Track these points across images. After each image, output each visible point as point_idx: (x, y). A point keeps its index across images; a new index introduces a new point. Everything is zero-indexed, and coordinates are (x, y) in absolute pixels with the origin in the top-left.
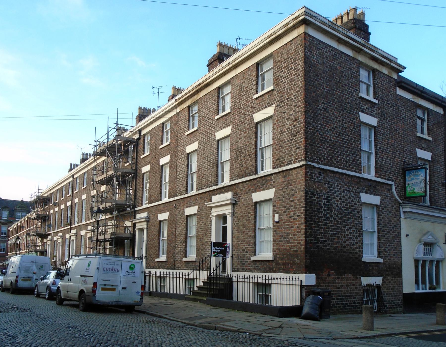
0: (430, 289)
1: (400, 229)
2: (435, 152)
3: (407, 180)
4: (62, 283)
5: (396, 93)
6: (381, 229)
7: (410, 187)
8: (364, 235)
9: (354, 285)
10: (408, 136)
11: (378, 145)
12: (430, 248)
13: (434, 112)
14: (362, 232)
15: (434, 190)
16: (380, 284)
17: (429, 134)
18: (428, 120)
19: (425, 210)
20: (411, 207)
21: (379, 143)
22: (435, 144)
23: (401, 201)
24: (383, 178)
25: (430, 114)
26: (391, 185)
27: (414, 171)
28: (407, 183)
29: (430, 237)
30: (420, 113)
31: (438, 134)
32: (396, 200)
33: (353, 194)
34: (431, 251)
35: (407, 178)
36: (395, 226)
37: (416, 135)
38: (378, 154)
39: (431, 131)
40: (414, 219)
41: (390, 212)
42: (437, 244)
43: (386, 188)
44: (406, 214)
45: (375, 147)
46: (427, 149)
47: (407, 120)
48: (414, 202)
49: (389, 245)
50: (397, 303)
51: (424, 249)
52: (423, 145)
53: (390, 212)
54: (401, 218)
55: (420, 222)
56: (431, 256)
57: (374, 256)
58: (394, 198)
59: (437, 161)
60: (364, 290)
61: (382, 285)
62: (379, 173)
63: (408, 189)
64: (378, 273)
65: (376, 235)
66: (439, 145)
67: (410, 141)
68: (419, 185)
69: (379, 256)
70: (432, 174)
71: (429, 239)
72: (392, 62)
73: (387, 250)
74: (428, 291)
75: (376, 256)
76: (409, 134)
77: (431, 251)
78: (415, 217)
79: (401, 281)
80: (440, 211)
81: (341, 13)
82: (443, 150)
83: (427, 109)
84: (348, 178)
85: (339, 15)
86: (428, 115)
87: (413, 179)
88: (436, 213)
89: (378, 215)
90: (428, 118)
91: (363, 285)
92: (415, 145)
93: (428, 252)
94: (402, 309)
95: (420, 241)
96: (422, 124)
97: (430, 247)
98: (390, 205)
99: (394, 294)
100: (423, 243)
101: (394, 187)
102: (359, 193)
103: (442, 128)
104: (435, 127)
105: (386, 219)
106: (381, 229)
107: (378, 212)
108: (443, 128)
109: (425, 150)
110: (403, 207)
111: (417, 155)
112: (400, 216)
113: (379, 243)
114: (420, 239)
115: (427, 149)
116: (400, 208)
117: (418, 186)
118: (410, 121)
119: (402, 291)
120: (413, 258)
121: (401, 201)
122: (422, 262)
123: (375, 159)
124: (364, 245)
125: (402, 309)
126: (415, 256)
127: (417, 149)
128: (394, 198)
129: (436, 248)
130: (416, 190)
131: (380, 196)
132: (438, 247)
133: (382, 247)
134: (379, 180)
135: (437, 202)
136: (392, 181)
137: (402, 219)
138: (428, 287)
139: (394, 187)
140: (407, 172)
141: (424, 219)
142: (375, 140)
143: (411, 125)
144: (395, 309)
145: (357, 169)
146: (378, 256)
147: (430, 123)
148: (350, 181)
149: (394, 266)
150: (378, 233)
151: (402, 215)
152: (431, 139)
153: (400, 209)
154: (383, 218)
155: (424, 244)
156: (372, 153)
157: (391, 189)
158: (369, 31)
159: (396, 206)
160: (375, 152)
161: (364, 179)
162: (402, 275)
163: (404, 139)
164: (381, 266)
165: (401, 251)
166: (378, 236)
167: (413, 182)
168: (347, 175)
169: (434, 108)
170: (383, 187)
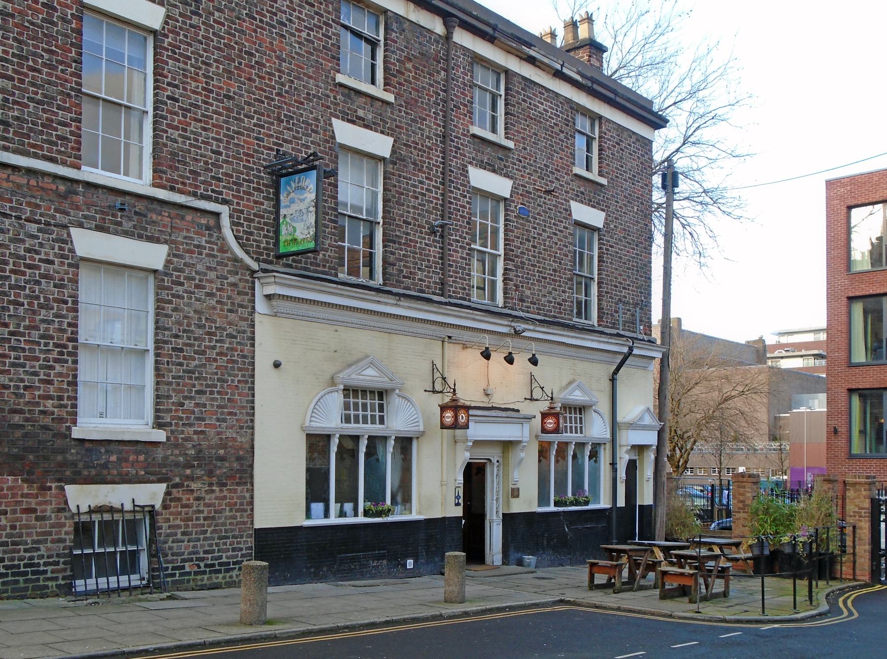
0: (366, 513)
1: (253, 345)
2: (408, 136)
3: (282, 204)
4: (195, 485)
6: (166, 342)
7: (287, 223)
8: (83, 357)
9: (29, 511)
10: (299, 79)
11: (166, 90)
12: (578, 416)
13: (406, 25)
14: (75, 348)
15: (400, 243)
16: (153, 506)
18: (386, 45)
19: (342, 295)
20: (277, 280)
21: (169, 84)
22: (407, 113)
23: (255, 266)
24: (181, 192)
25: (394, 26)
26: (217, 215)
27: (296, 177)
28: (283, 211)
29: (577, 393)
30: (582, 123)
31: (424, 88)
32: (236, 259)
33: (33, 228)
34: (581, 423)
35: (282, 198)
36: (230, 336)
37: (572, 171)
39: (395, 76)
41: (210, 295)
42: (594, 407)
43: (193, 222)
44: (274, 303)
45: (156, 95)
46: (374, 123)
47: (300, 31)
48: (317, 272)
49: (199, 392)
50: (227, 557)
52: (361, 113)
53: (210, 295)
54: (256, 315)
56: (581, 432)
57: (144, 422)
58: (229, 255)
59: (414, 164)
60: (76, 523)
61: (165, 506)
62: (165, 173)
63: (283, 230)
64: (146, 473)
65: (150, 359)
66: (425, 120)
67: (308, 94)
68: (305, 217)
69: (159, 424)
70: (394, 197)
71: (369, 377)
73: (189, 405)
74: (552, 508)
75: (150, 424)
76: (304, 74)
77: (581, 423)
78: (311, 314)
80: (399, 300)
82: (437, 135)
83: (507, 71)
84: (12, 177)
86: (386, 29)
87: (292, 201)
88: (386, 304)
89: (160, 302)
90: (386, 39)
91: (74, 510)
92: (329, 107)
93: (574, 425)
95: (332, 382)
96: (589, 149)
97: (580, 414)
98: (212, 275)
99: (214, 531)
100: (342, 387)
101: (225, 221)
102: (65, 227)
103: (438, 72)
104: (409, 66)
105: (192, 314)
106: (166, 342)
107: (160, 287)
108: (443, 73)
109: (366, 126)
110: (262, 281)
111: (333, 137)
112: (253, 308)
113: (158, 383)
114: (332, 378)
115: (374, 123)
116: (253, 283)
117: (302, 220)
118: (309, 35)
119: (252, 523)
120: (303, 429)
121: (255, 266)
122: (573, 447)
123: (155, 130)
124: (80, 388)
126: (307, 424)
127: (334, 120)
128: (229, 255)
129: (395, 403)
130: (299, 235)
131: (166, 242)
132: (594, 414)
133: (169, 397)
134: (162, 194)
135: (409, 278)
136: (225, 202)
137: (257, 318)
138: (361, 510)
139: (225, 221)
140: (283, 180)
141: (597, 358)
142: (155, 74)
143: (314, 49)
144: (220, 576)
145: (59, 152)
146: (154, 423)
147: (393, 52)
148: (19, 186)
149: (222, 452)
150: (157, 355)
151: (261, 306)
152: (390, 98)
153: (253, 289)
154: (175, 310)
156: (147, 112)
157: (219, 227)
159: (239, 276)
160: (155, 109)
161: (88, 185)
162: (252, 477)
163: (283, 85)
164: (160, 453)
165: (253, 408)
166: (157, 362)
167: (295, 207)
168: (15, 168)
169: (407, 11)
170: (183, 218)
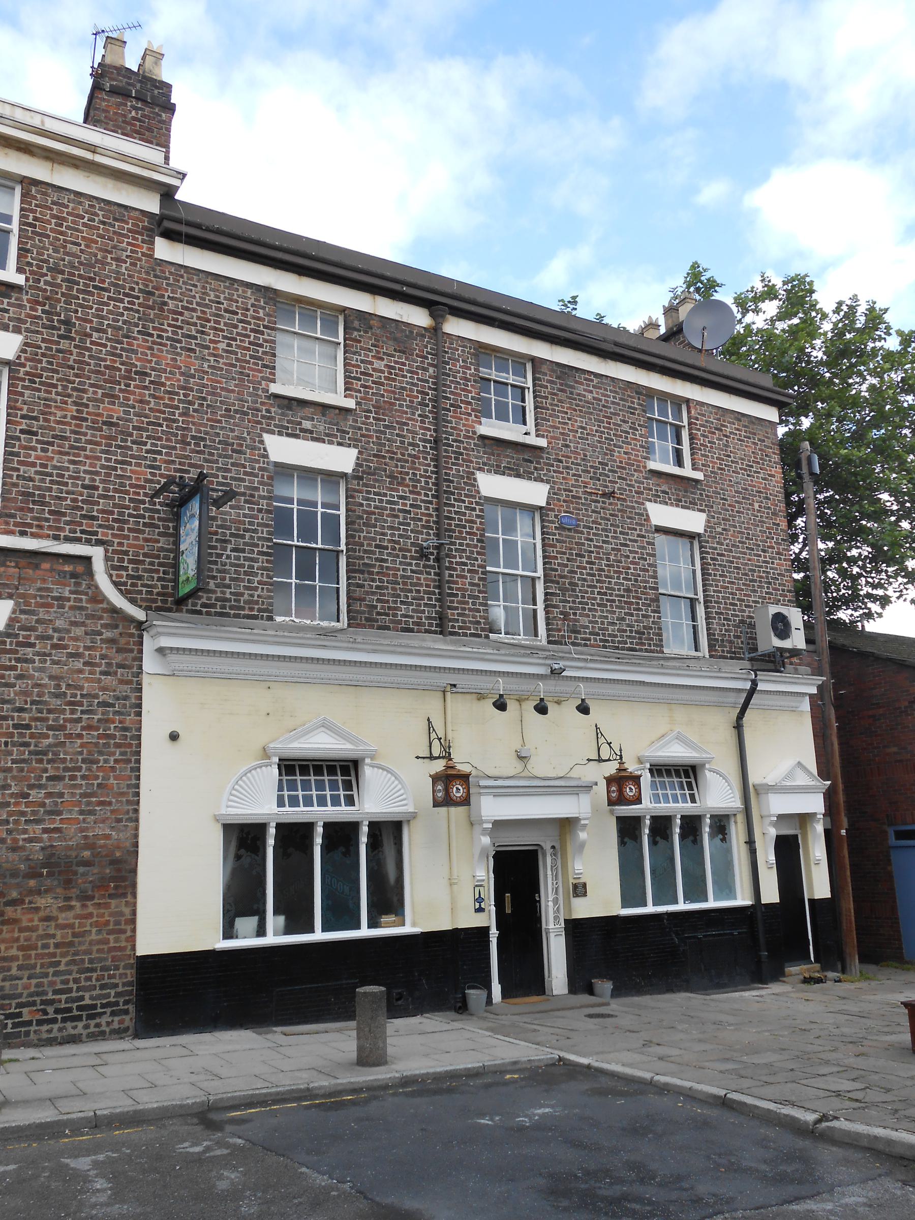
5: (151, 256)
17: (695, 468)
26: (88, 560)
37: (645, 467)
38: (708, 553)
40: (228, 677)
51: (280, 781)
55: (269, 684)
72: (99, 150)
79: (127, 911)
81: (886, 310)
85: (815, 288)
94: (127, 1018)
95: (265, 753)
100: (648, 766)
101: (99, 566)
125: (128, 1021)
128: (105, 606)
151: (150, 663)
155: (651, 771)
157: (90, 573)
158: (172, 101)
162: (134, 885)
